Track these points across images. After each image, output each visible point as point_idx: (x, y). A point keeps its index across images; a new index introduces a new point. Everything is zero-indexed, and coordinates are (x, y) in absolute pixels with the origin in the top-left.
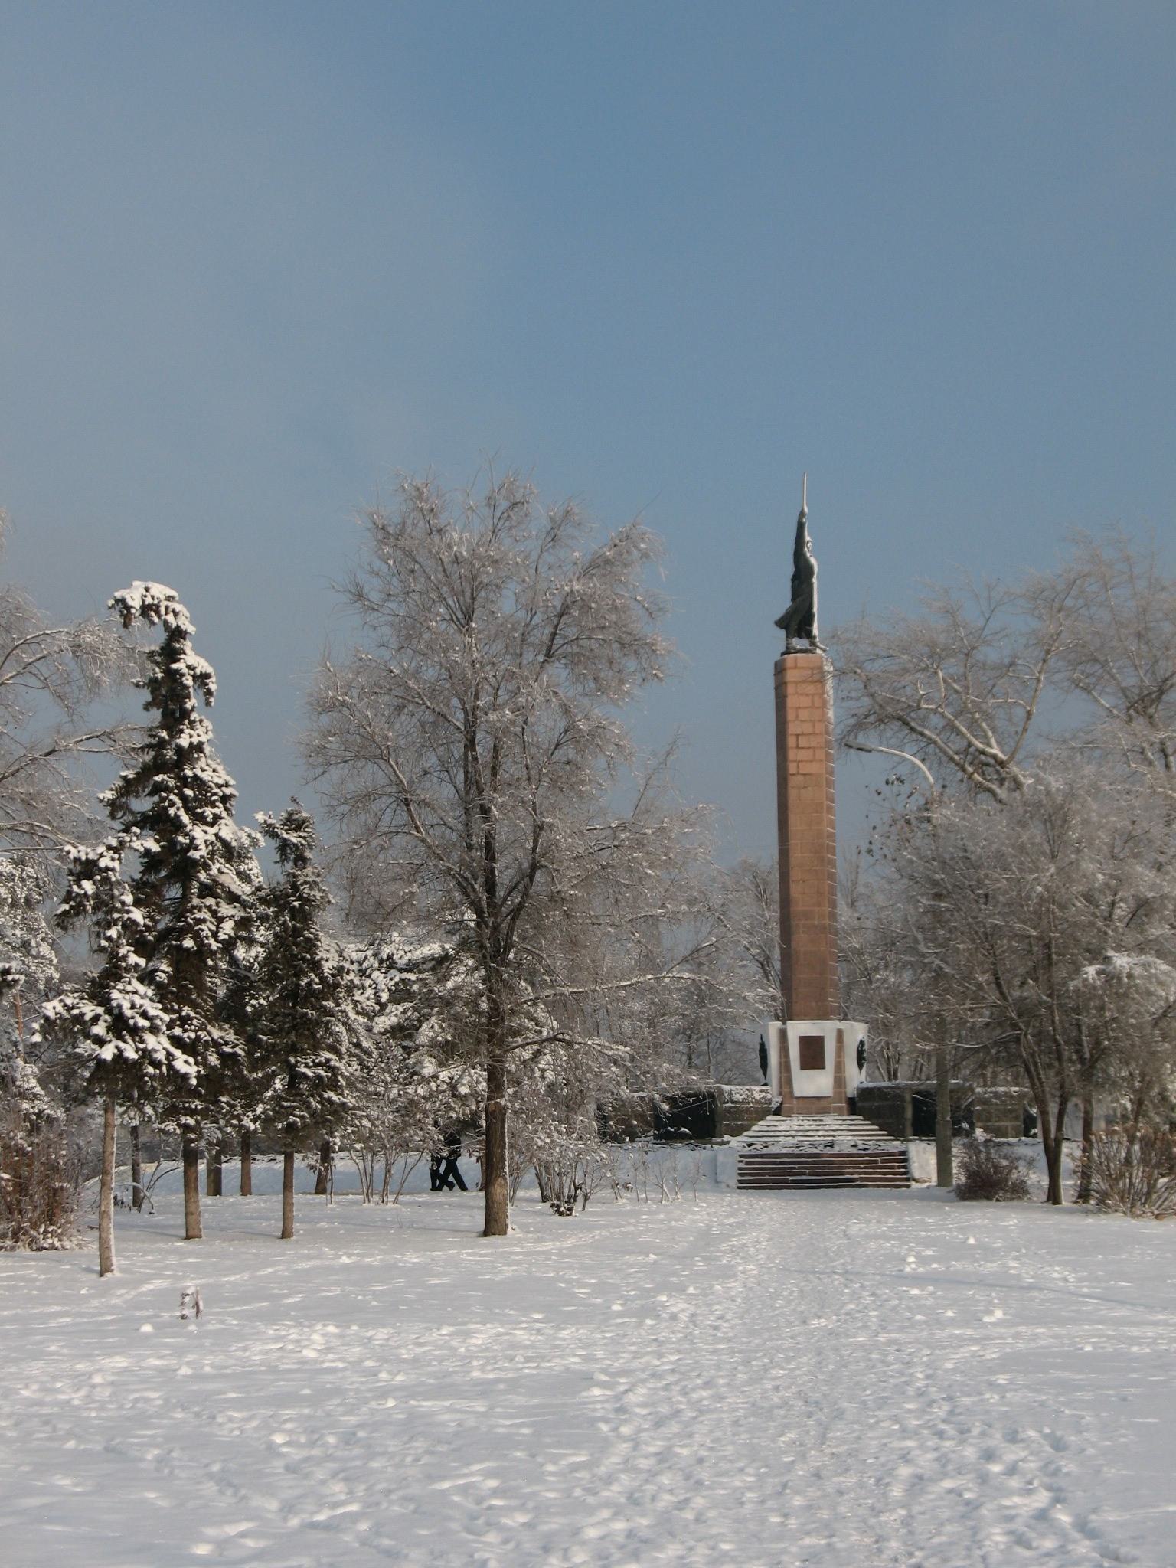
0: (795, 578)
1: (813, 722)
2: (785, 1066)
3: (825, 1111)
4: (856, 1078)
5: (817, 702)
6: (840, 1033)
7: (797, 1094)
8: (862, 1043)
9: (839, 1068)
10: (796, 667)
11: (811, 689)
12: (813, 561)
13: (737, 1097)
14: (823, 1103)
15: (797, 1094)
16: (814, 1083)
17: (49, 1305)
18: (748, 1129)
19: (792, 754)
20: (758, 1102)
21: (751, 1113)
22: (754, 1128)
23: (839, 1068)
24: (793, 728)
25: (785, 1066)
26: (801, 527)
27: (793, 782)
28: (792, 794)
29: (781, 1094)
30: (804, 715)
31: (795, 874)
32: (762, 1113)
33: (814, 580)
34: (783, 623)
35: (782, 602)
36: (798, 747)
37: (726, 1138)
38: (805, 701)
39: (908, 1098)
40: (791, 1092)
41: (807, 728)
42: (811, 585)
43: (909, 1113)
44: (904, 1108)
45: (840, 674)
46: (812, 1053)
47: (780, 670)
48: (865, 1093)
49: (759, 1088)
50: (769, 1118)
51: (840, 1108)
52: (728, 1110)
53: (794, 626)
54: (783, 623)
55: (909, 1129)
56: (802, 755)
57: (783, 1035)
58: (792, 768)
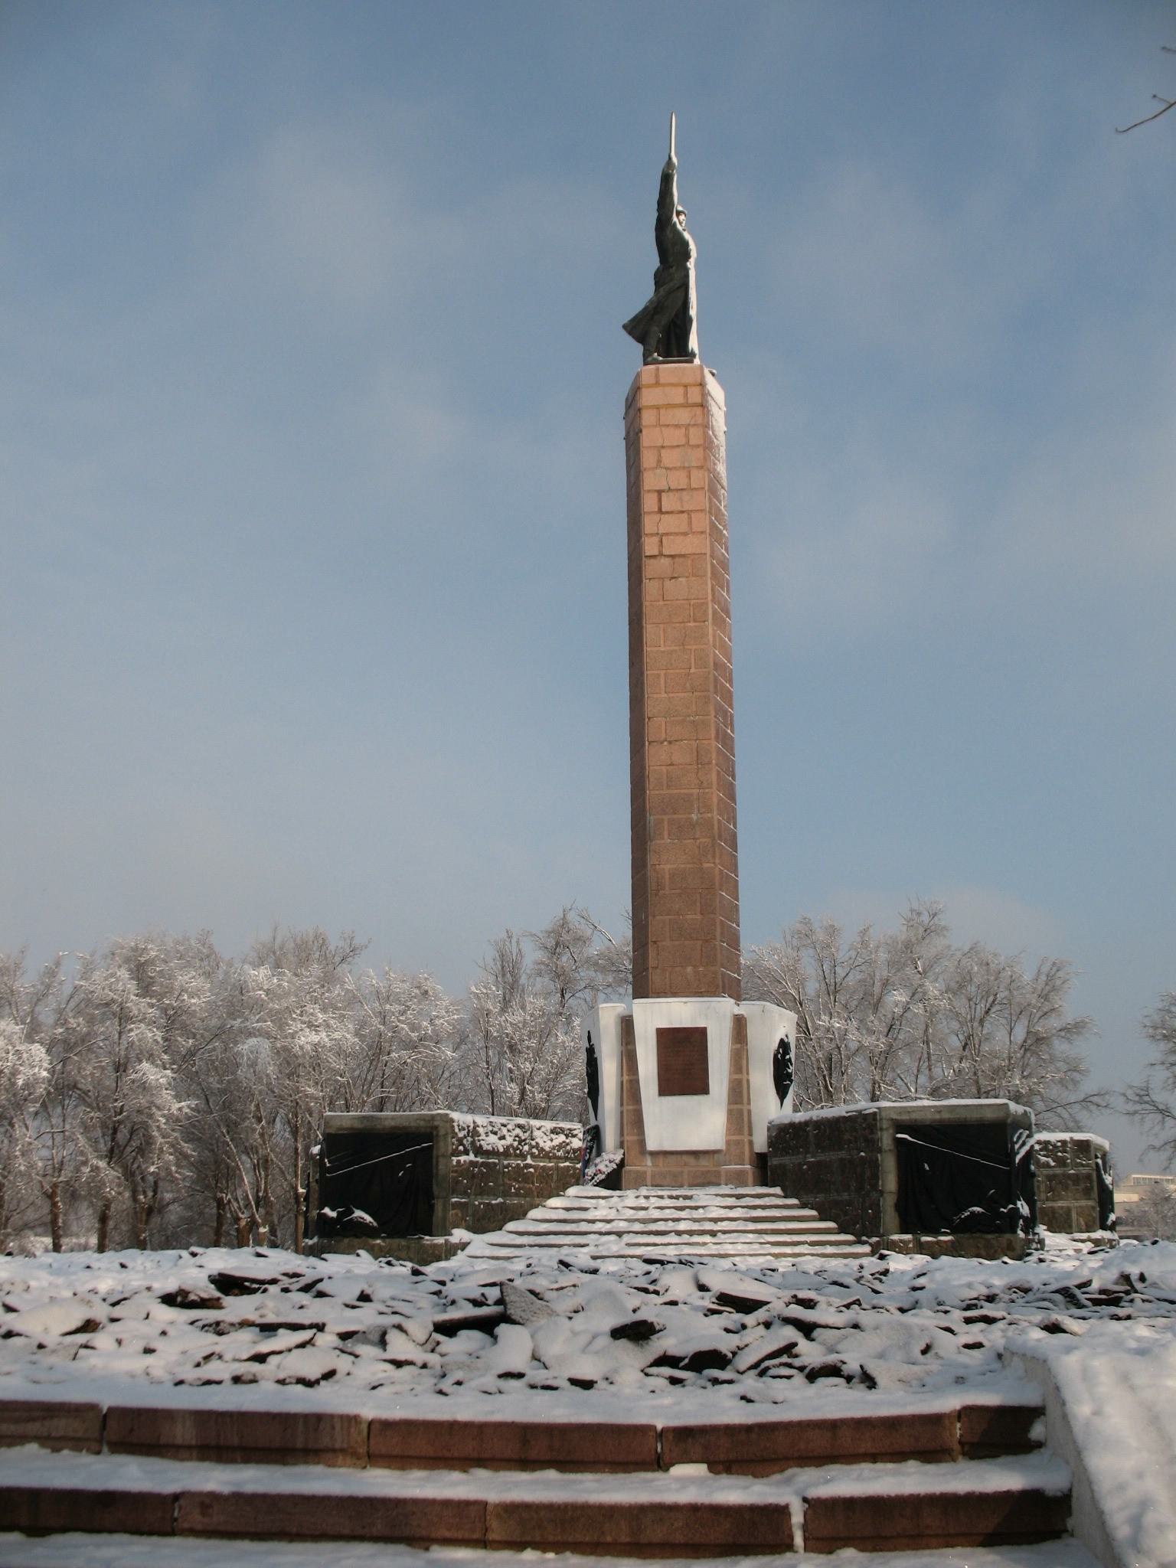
0: (659, 220)
1: (688, 470)
2: (631, 1091)
3: (706, 1180)
4: (770, 1109)
5: (695, 436)
6: (740, 1023)
7: (652, 1145)
8: (784, 1045)
9: (739, 1094)
10: (657, 384)
11: (683, 416)
12: (687, 236)
13: (490, 1142)
14: (705, 1163)
15: (652, 1145)
16: (694, 1124)
17: (947, 1097)
18: (520, 1214)
19: (649, 524)
20: (545, 1155)
21: (527, 1178)
22: (534, 1213)
23: (739, 1094)
24: (651, 481)
25: (631, 1091)
26: (666, 179)
27: (650, 568)
28: (650, 589)
29: (621, 1145)
30: (670, 458)
31: (656, 728)
32: (556, 1182)
33: (691, 264)
34: (638, 328)
35: (641, 293)
36: (660, 511)
37: (459, 1235)
38: (676, 437)
39: (886, 1140)
40: (642, 1143)
41: (678, 479)
42: (687, 270)
43: (890, 1182)
44: (875, 1166)
45: (710, 763)
46: (683, 1062)
47: (632, 406)
48: (785, 1136)
49: (549, 1125)
50: (572, 1191)
51: (742, 1173)
52: (466, 1170)
53: (656, 333)
54: (638, 328)
55: (890, 1216)
56: (669, 523)
57: (627, 1025)
58: (650, 546)
